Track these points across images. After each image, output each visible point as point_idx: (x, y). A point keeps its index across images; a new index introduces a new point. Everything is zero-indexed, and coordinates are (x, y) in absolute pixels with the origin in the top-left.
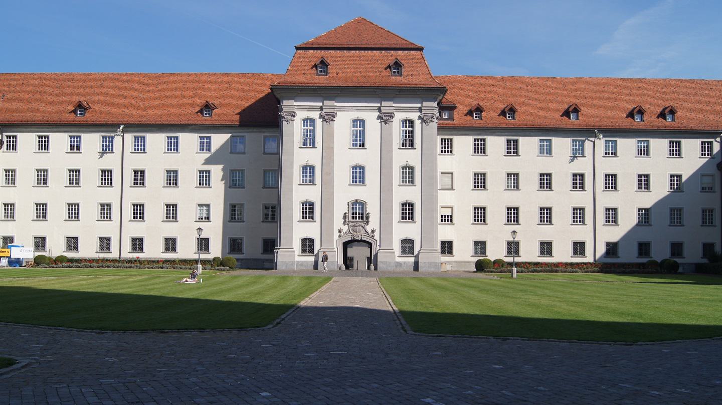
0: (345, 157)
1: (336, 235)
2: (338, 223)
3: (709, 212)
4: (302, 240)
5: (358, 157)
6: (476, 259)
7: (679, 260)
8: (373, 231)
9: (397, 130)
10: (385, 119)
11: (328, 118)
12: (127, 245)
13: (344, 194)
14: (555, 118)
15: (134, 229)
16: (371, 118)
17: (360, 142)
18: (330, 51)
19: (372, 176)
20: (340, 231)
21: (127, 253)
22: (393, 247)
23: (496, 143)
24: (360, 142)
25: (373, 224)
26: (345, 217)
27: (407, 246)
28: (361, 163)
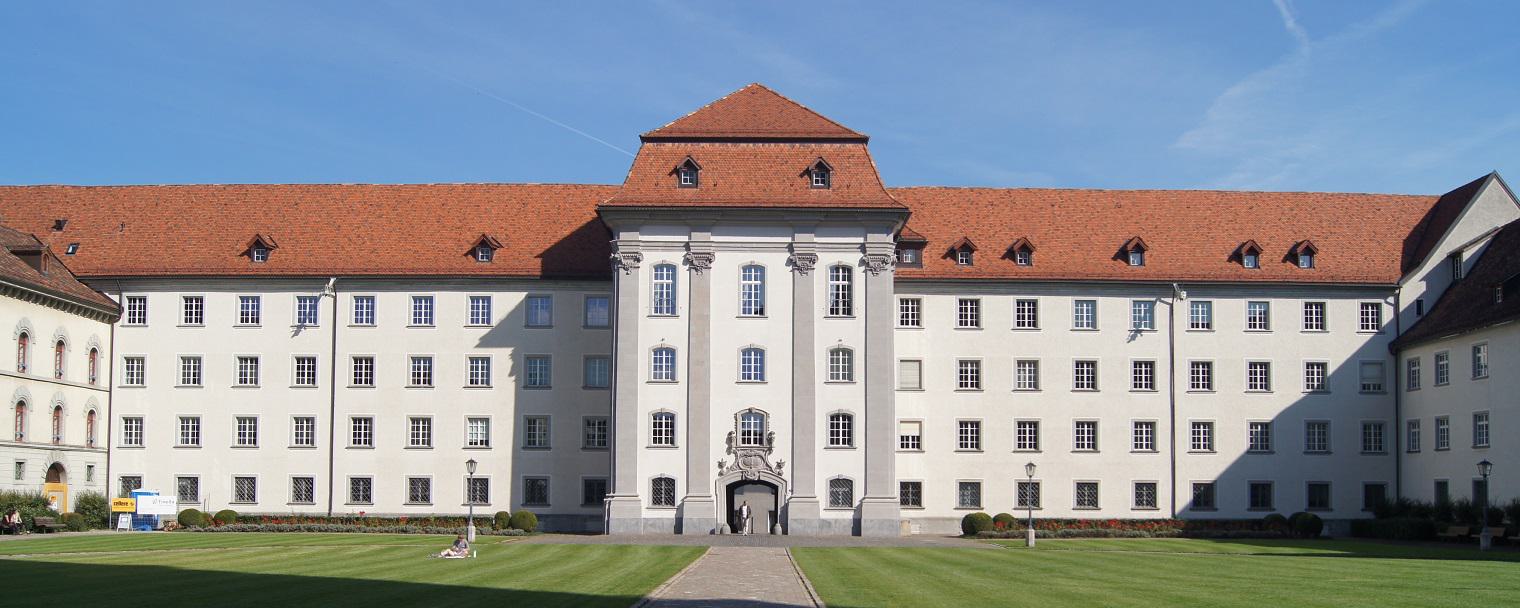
0: (730, 333)
1: (714, 471)
2: (718, 450)
3: (1375, 428)
4: (831, 481)
5: (754, 332)
6: (963, 514)
7: (1322, 515)
8: (779, 465)
9: (821, 284)
10: (801, 264)
11: (699, 263)
12: (343, 491)
13: (728, 399)
14: (1102, 263)
15: (355, 463)
16: (776, 264)
17: (755, 307)
18: (702, 144)
19: (724, 364)
20: (721, 465)
21: (343, 506)
22: (816, 494)
23: (998, 308)
24: (755, 307)
25: (781, 452)
26: (729, 440)
27: (841, 490)
28: (758, 344)
